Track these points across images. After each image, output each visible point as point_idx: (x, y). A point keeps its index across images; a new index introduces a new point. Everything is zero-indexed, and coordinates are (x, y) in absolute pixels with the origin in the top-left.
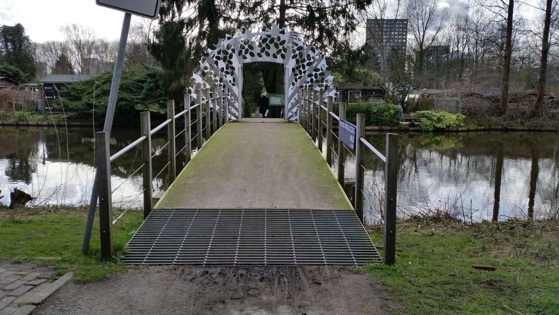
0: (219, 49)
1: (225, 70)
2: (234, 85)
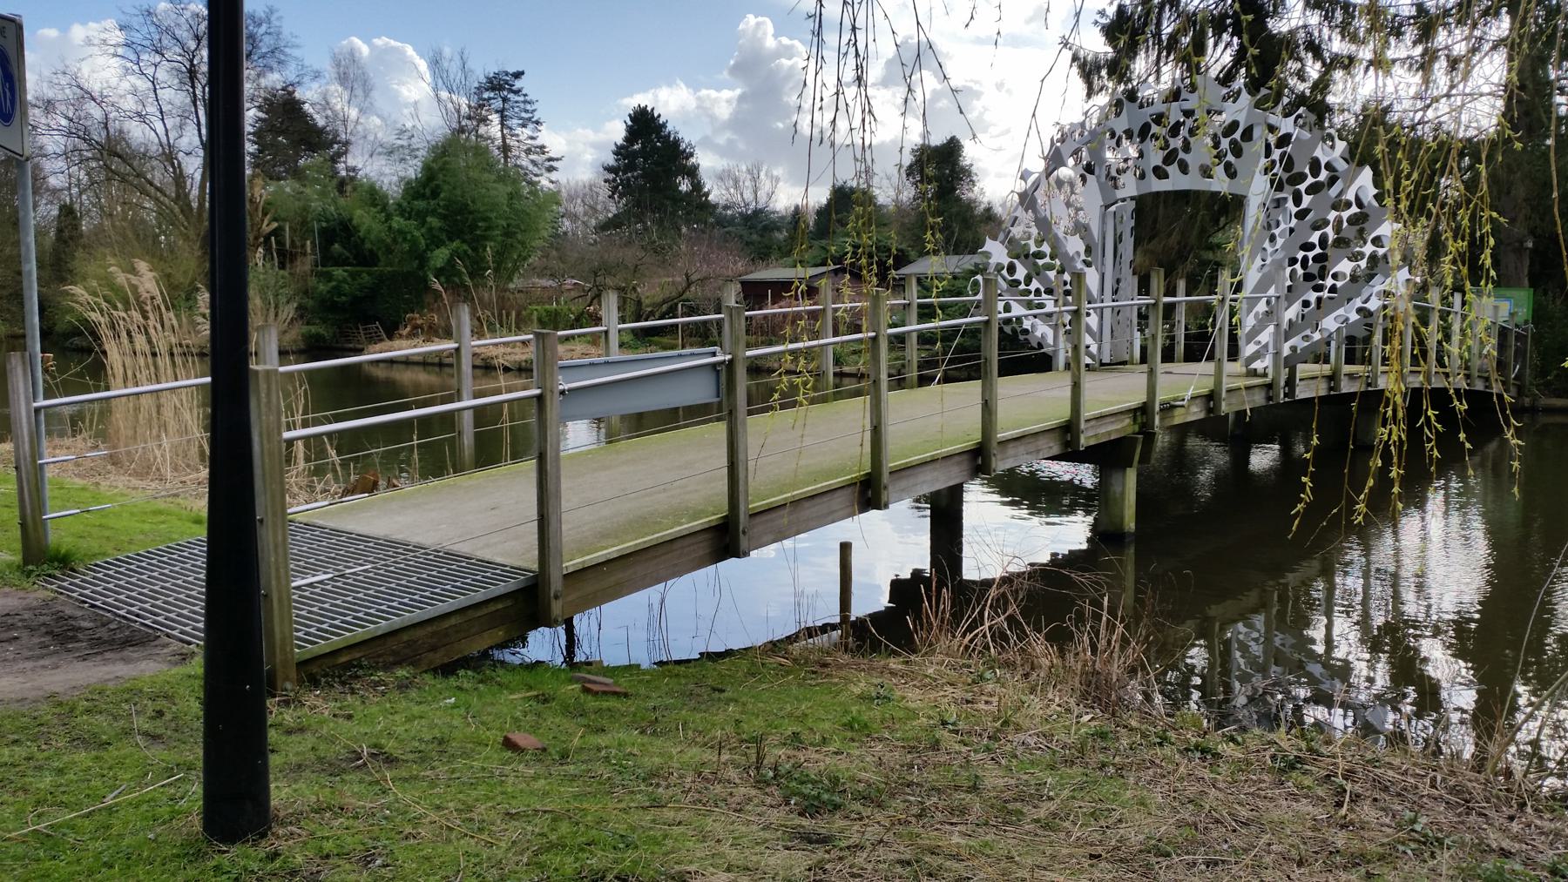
2: (1088, 264)
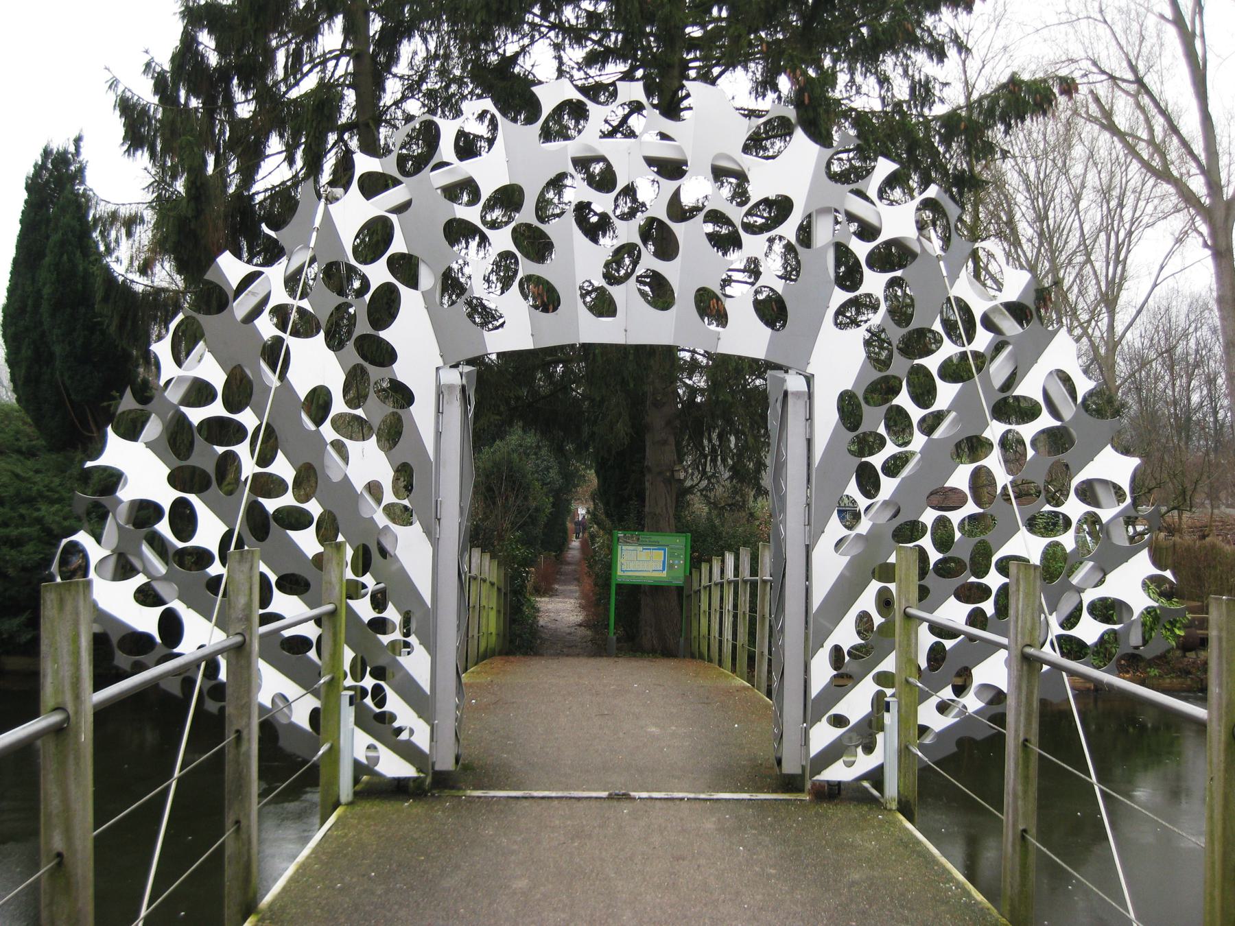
1: (339, 406)
2: (402, 516)
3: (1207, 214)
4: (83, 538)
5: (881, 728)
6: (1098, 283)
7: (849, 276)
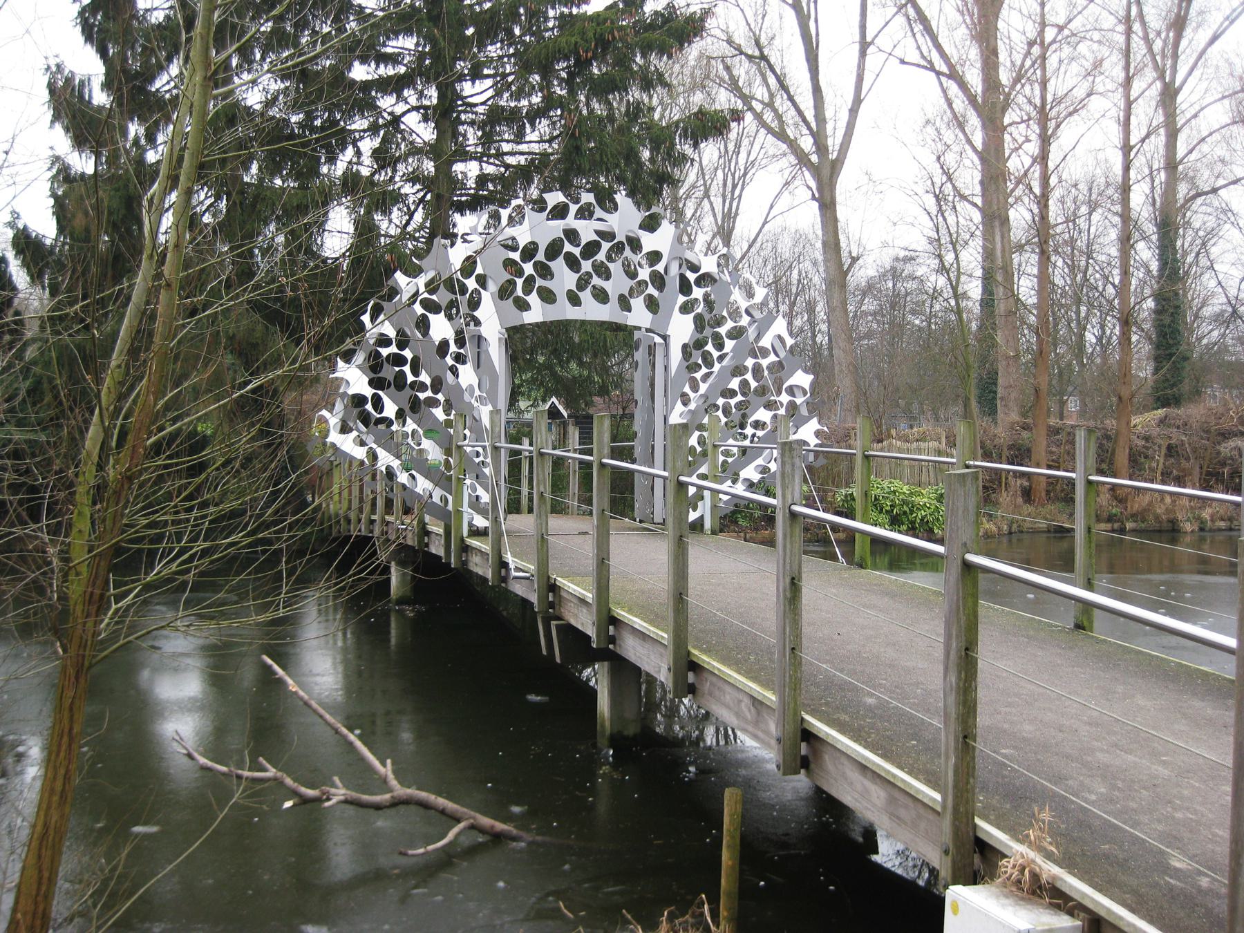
0: (431, 274)
3: (816, 171)
4: (324, 413)
5: (702, 498)
6: (715, 215)
7: (685, 287)
